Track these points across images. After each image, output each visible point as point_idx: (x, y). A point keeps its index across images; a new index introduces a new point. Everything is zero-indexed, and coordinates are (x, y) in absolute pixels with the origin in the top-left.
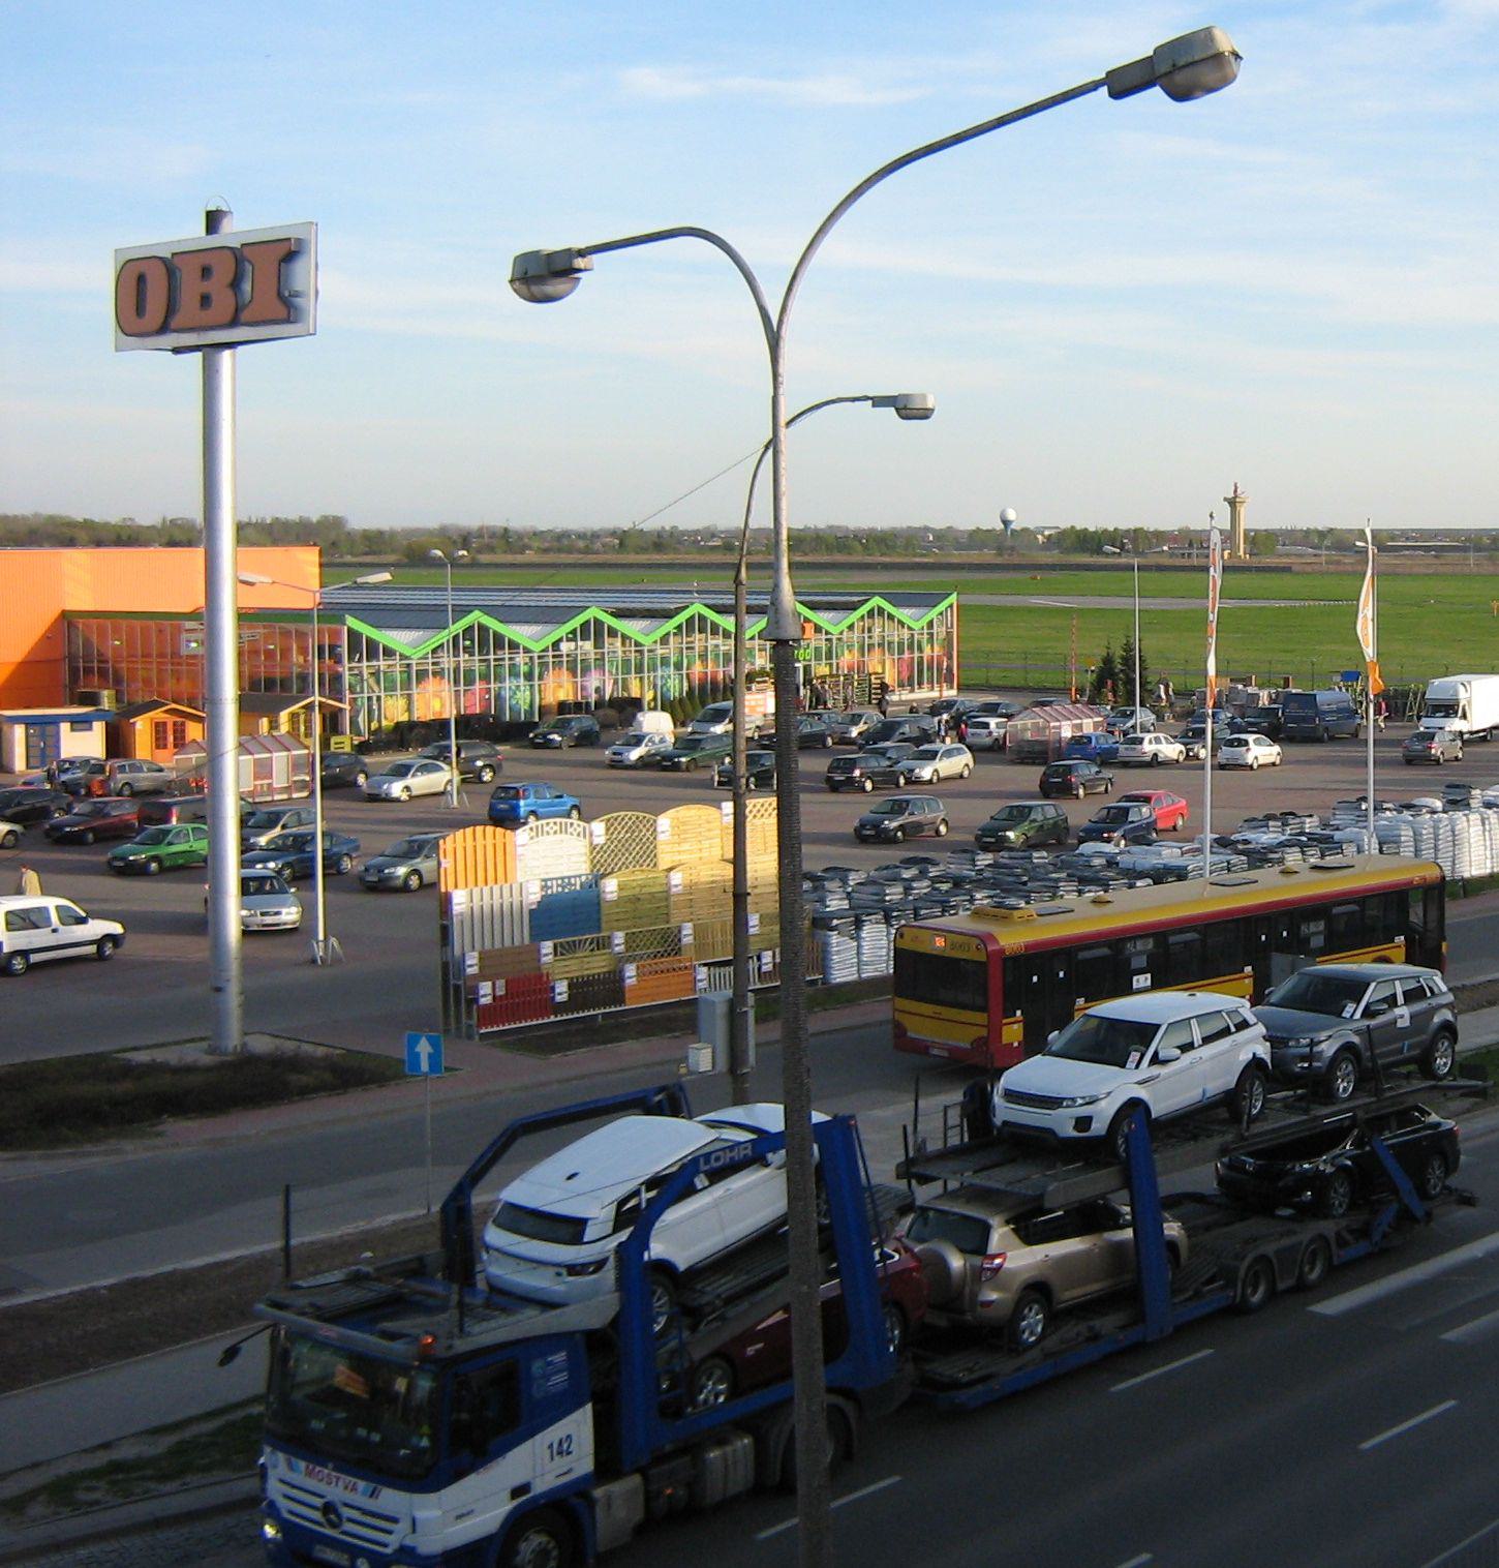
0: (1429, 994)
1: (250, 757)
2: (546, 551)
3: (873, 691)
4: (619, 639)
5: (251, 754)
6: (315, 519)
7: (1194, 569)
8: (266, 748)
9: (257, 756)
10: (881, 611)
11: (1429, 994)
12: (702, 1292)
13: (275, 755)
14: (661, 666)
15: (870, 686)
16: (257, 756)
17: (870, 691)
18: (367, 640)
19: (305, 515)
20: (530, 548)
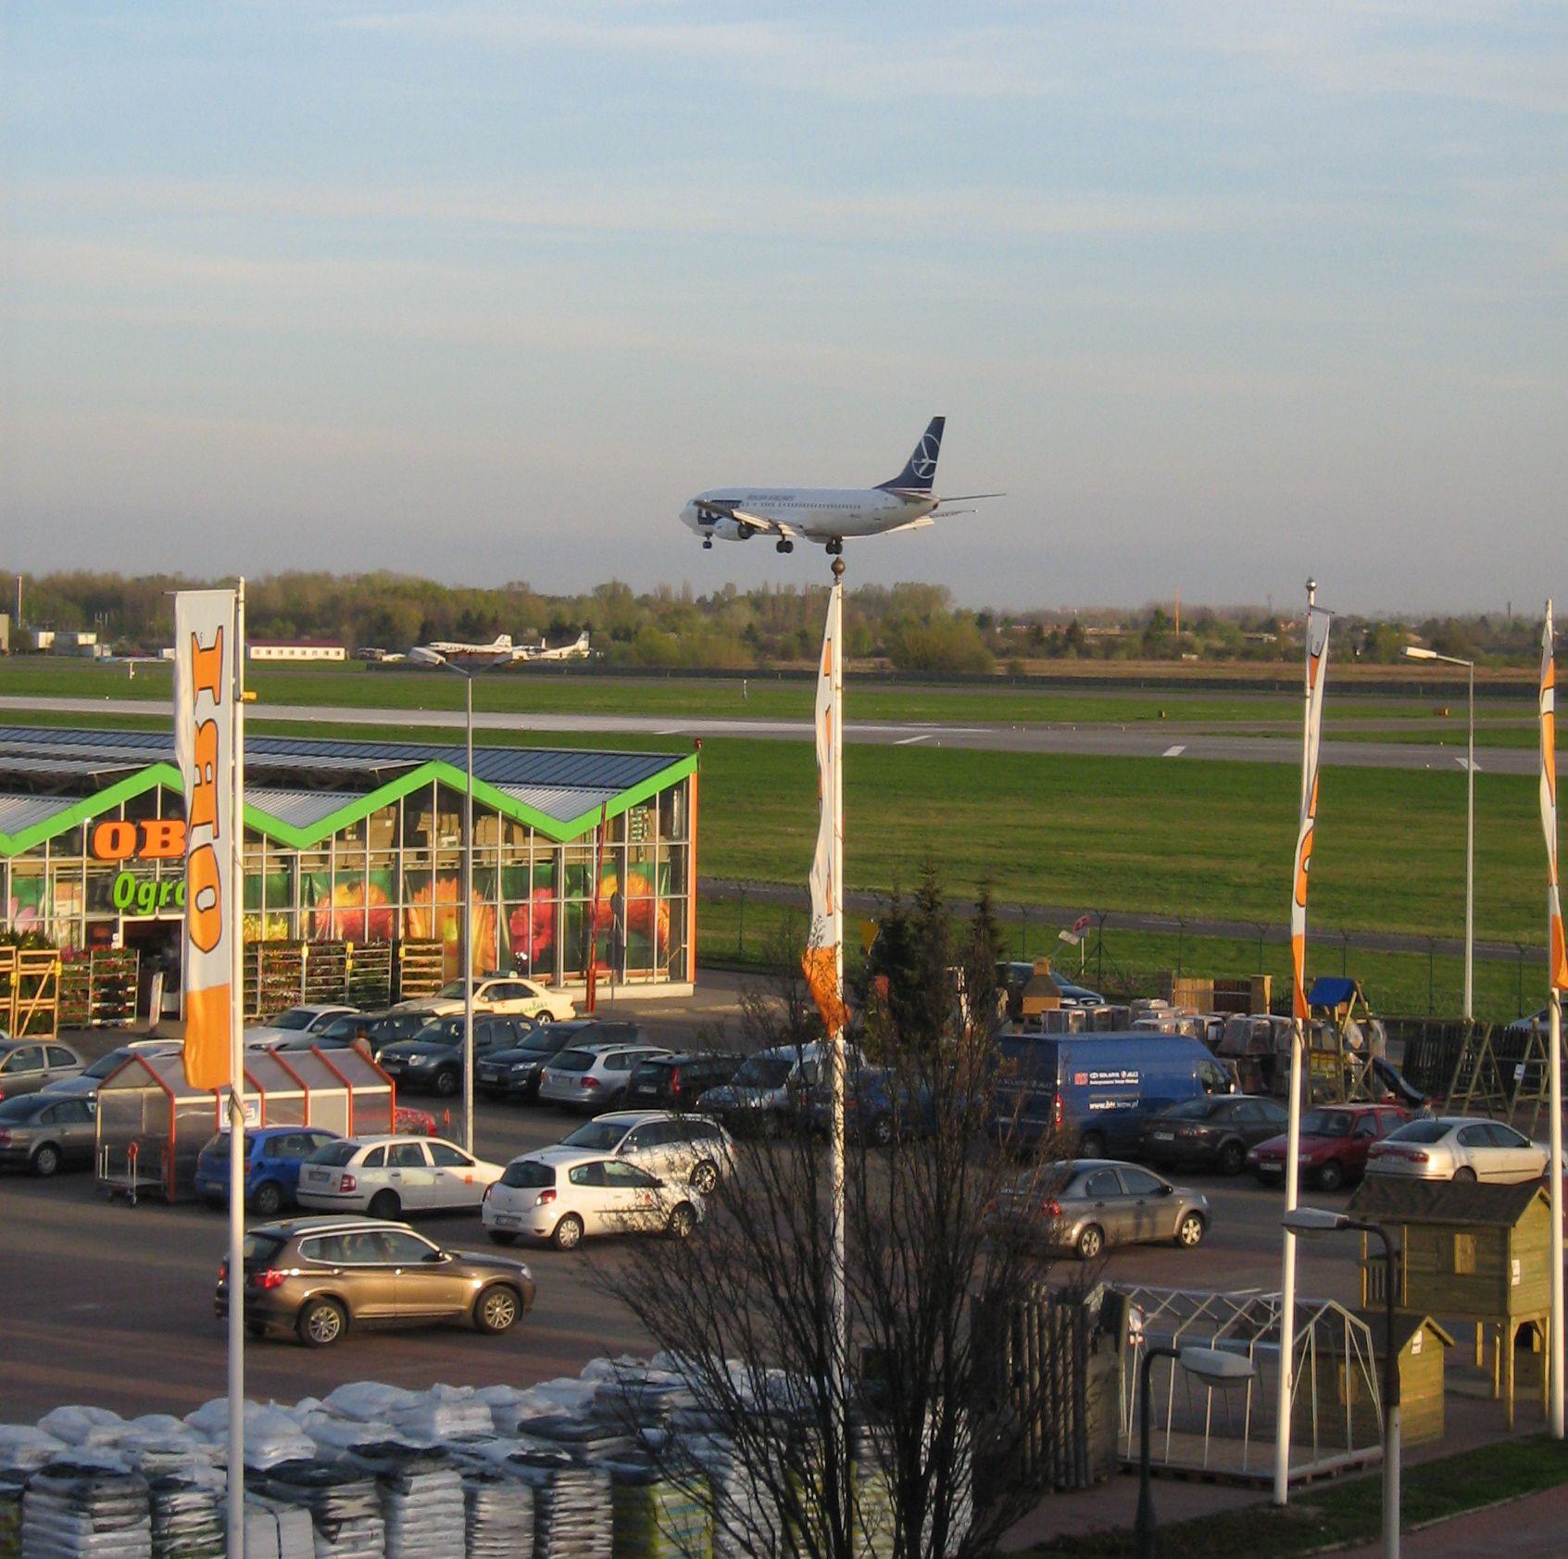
0: (1049, 1094)
1: (345, 1091)
2: (1220, 655)
3: (403, 982)
4: (500, 827)
5: (346, 1085)
6: (889, 587)
7: (1267, 686)
8: (293, 1076)
9: (356, 1091)
10: (452, 800)
11: (1049, 1094)
12: (1195, 1224)
13: (312, 1093)
14: (670, 846)
15: (396, 968)
16: (356, 1091)
17: (395, 981)
18: (474, 802)
19: (875, 582)
20: (1190, 648)
